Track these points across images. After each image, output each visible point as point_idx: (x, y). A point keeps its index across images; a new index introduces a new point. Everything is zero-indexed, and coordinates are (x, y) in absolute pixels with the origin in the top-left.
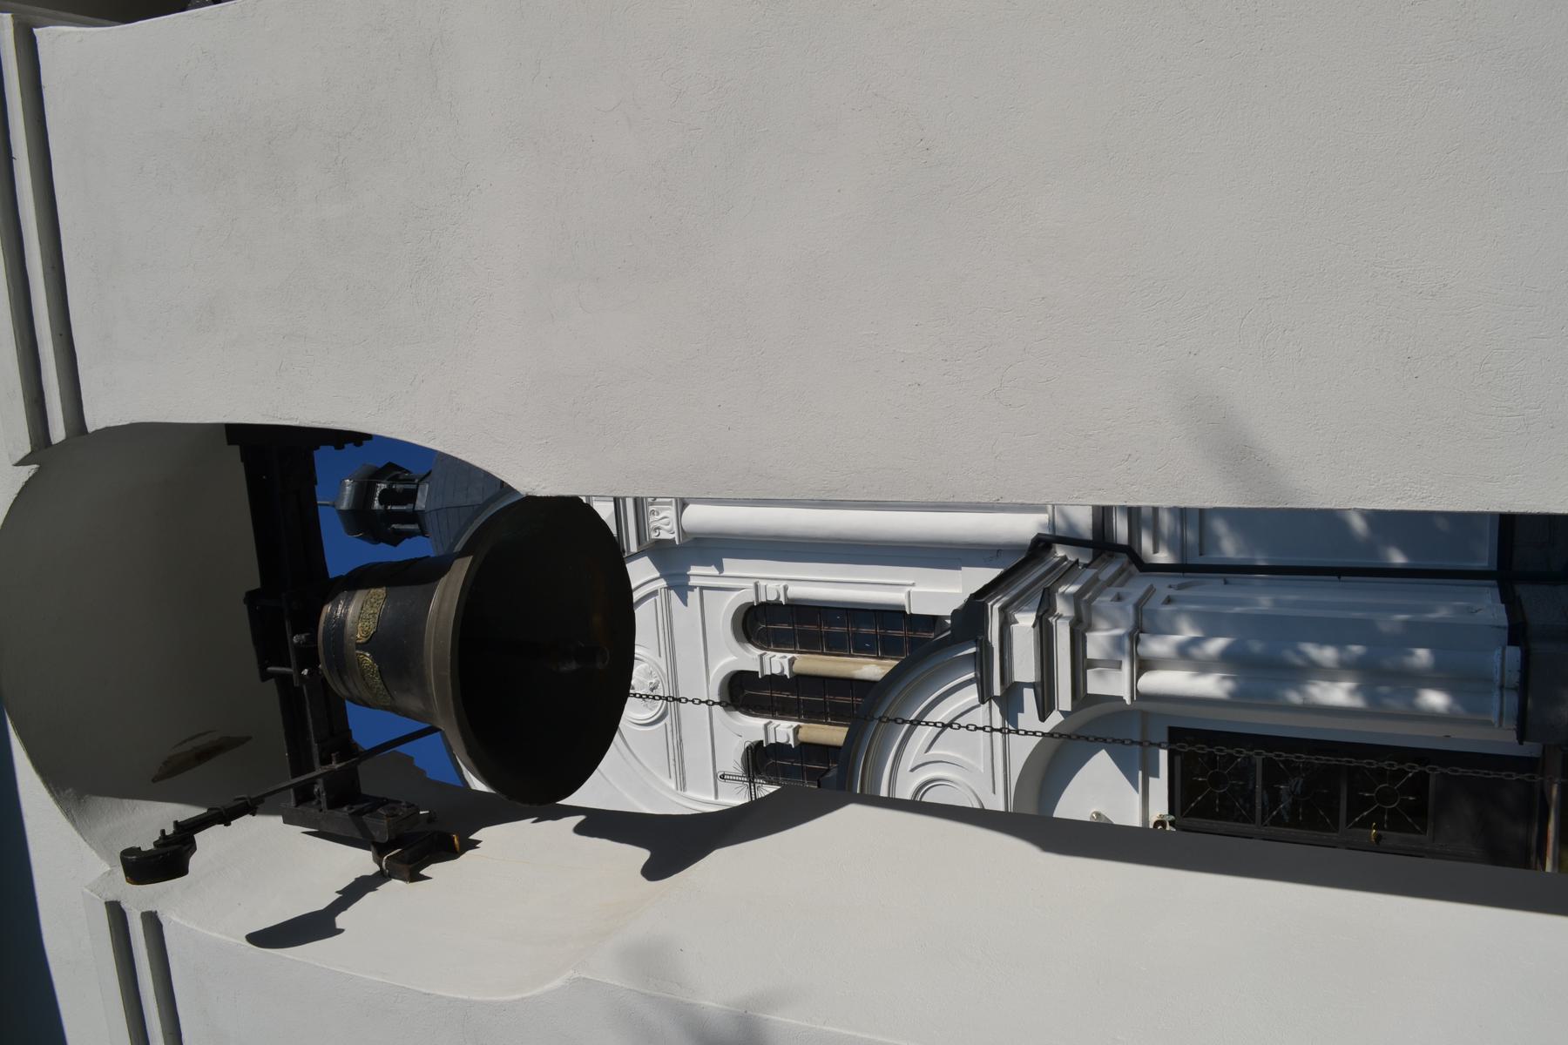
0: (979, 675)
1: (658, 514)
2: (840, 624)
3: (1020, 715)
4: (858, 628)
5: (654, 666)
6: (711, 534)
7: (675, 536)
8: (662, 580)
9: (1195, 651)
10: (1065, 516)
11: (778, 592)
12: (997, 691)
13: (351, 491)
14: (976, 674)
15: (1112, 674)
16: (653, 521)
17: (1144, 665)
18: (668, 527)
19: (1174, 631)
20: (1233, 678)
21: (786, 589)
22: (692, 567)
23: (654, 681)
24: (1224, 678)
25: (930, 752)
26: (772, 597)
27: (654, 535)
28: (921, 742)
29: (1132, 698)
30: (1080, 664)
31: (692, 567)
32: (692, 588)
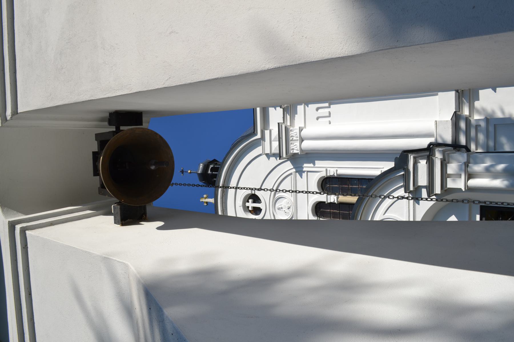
0: (405, 184)
1: (293, 144)
2: (356, 184)
3: (296, 115)
4: (362, 186)
5: (290, 200)
6: (312, 150)
7: (299, 151)
8: (294, 169)
9: (492, 169)
10: (441, 137)
11: (334, 172)
12: (411, 188)
13: (202, 167)
14: (404, 184)
15: (458, 180)
16: (292, 146)
17: (470, 176)
18: (296, 149)
19: (483, 163)
20: (507, 180)
21: (337, 171)
22: (304, 164)
23: (289, 205)
24: (504, 180)
25: (385, 215)
26: (332, 174)
27: (291, 152)
28: (382, 211)
29: (465, 188)
30: (444, 176)
31: (304, 164)
32: (304, 172)
